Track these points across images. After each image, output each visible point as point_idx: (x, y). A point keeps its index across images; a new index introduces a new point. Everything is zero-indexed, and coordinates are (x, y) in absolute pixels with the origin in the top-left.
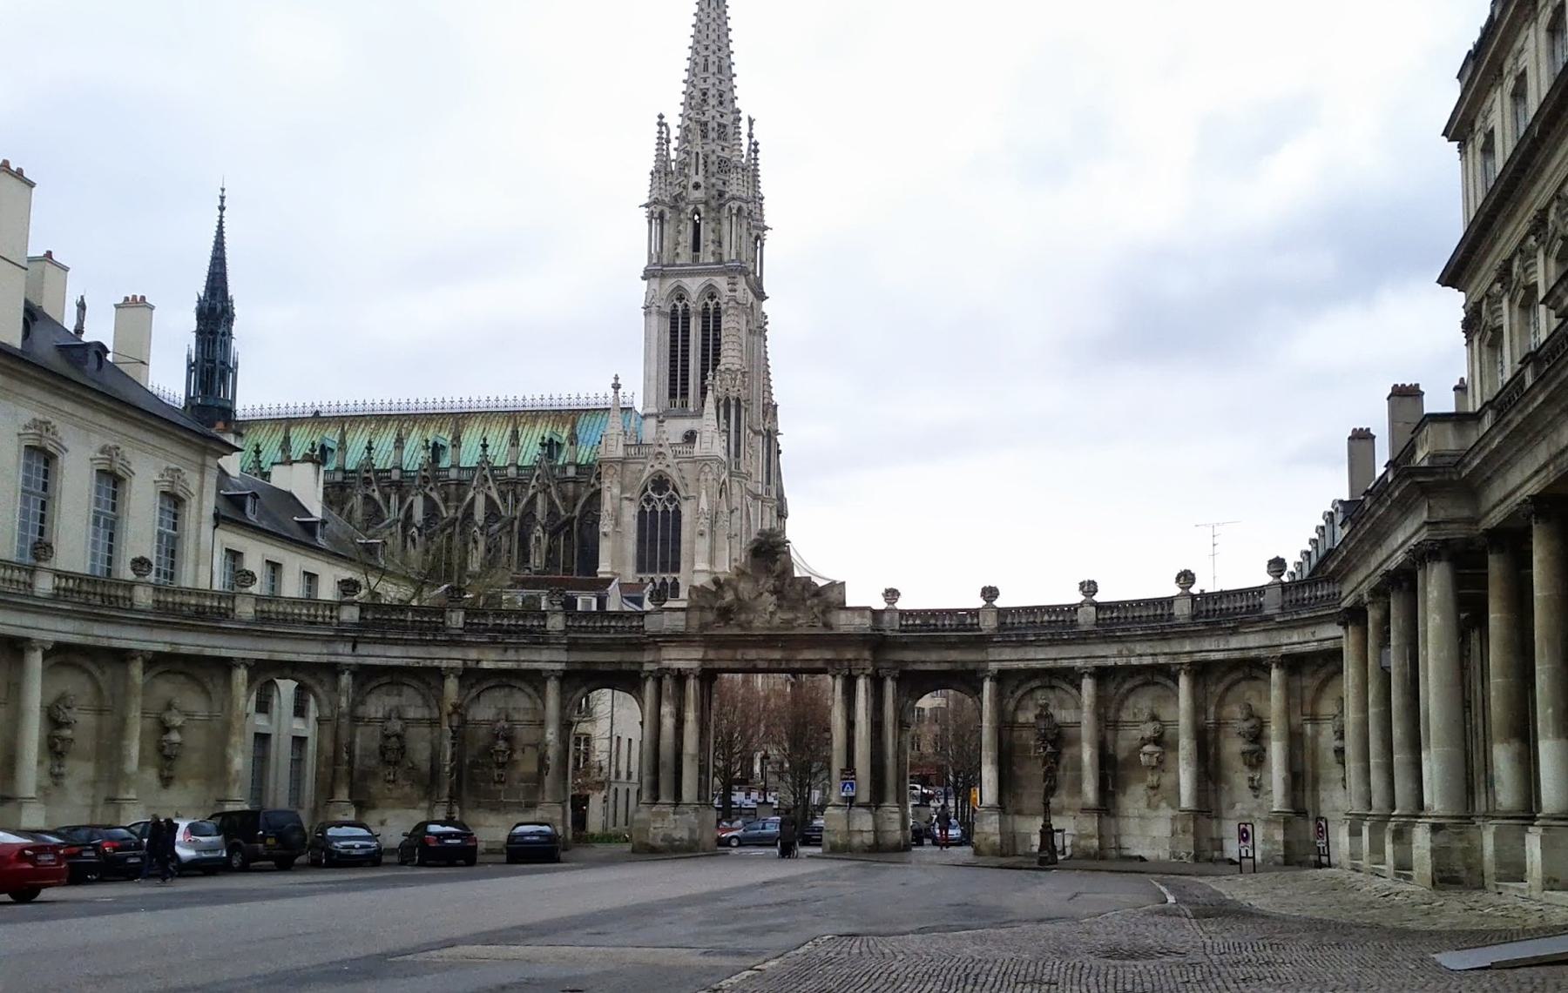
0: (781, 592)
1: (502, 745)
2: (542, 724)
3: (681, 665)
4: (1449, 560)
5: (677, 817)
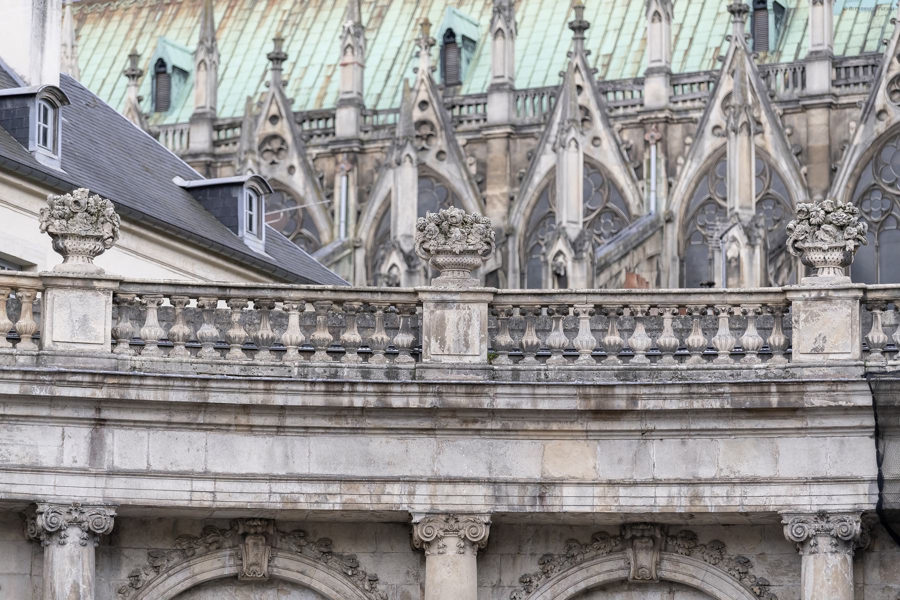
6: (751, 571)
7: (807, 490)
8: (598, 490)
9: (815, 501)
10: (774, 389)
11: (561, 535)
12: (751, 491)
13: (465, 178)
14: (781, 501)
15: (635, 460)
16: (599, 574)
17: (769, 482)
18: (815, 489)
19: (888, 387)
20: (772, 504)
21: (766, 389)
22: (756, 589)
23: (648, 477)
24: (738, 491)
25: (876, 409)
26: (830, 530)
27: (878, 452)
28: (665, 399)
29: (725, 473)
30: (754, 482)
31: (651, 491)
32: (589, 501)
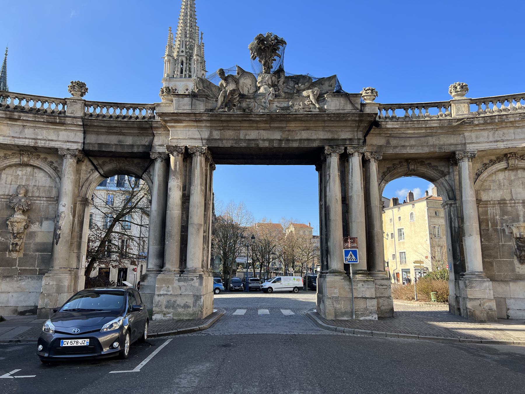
0: (276, 85)
1: (18, 216)
2: (57, 199)
3: (189, 144)
4: (414, 188)
5: (182, 284)
6: (53, 165)
7: (65, 144)
8: (9, 138)
9: (67, 146)
10: (57, 118)
11: (4, 152)
12: (51, 142)
13: (47, 124)
14: (59, 146)
15: (21, 133)
16: (13, 162)
17: (56, 141)
18: (68, 144)
19: (87, 120)
20: (56, 146)
21: (55, 118)
22: (54, 169)
23: (24, 137)
24: (48, 142)
25: (83, 125)
26: (70, 153)
27: (84, 137)
28: (29, 117)
29: (45, 138)
30: (52, 140)
31: (24, 140)
32: (6, 141)
